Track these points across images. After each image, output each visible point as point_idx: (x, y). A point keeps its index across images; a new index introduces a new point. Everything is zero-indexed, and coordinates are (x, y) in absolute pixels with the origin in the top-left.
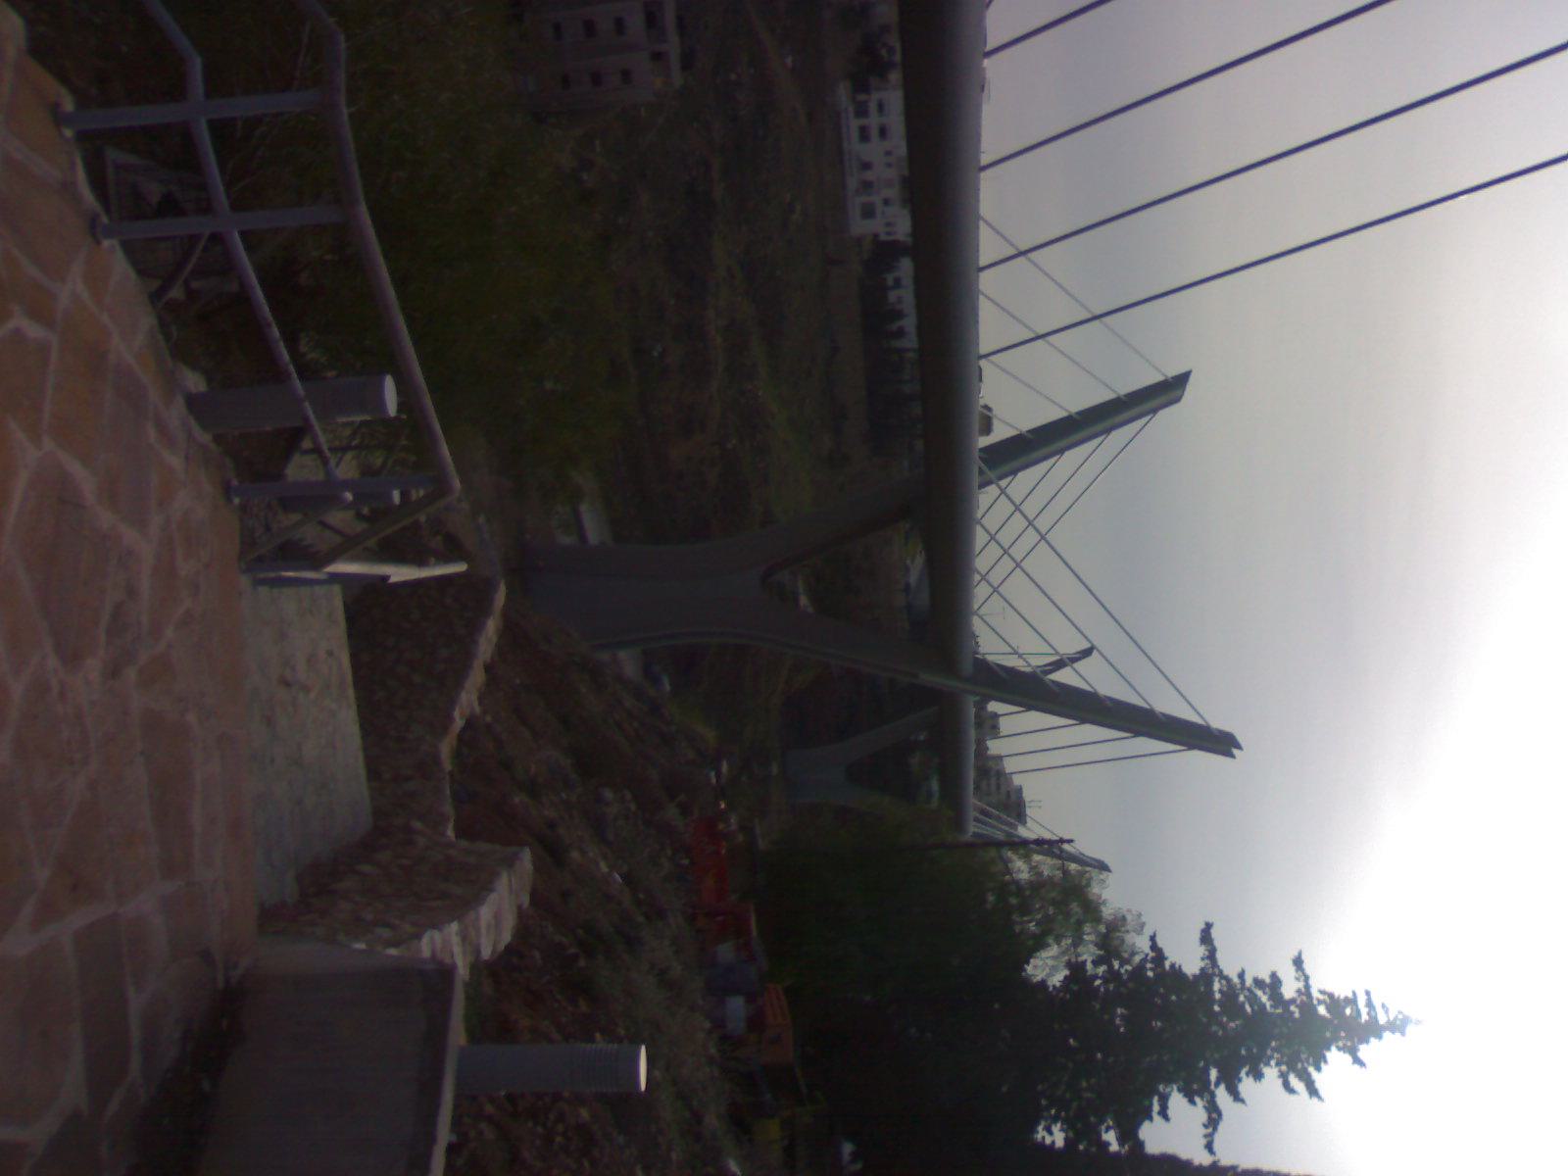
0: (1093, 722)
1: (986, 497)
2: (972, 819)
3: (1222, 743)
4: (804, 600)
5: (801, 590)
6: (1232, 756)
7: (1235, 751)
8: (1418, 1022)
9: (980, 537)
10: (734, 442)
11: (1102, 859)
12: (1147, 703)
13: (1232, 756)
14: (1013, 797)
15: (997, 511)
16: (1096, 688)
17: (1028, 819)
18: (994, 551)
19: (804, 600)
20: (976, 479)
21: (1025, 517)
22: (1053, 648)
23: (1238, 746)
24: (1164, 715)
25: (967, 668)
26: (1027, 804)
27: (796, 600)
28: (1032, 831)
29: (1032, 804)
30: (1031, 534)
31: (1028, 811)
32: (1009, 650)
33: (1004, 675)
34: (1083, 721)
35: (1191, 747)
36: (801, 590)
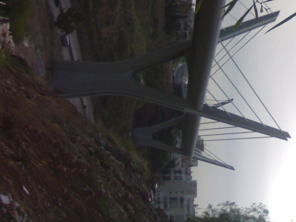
0: (241, 127)
1: (219, 47)
2: (194, 150)
3: (232, 168)
4: (142, 81)
5: (141, 77)
6: (287, 140)
7: (288, 138)
8: (193, 172)
9: (214, 63)
10: (123, 28)
11: (231, 165)
12: (242, 115)
13: (287, 140)
14: (200, 143)
15: (220, 51)
16: (226, 110)
17: (205, 149)
18: (217, 67)
19: (142, 81)
20: (217, 41)
21: (226, 51)
22: (214, 98)
23: (290, 137)
24: (283, 131)
25: (201, 107)
26: (205, 145)
27: (140, 80)
28: (211, 157)
29: (206, 145)
30: (228, 57)
31: (205, 147)
32: (214, 99)
33: (231, 116)
34: (219, 121)
35: (272, 136)
36: (141, 77)
